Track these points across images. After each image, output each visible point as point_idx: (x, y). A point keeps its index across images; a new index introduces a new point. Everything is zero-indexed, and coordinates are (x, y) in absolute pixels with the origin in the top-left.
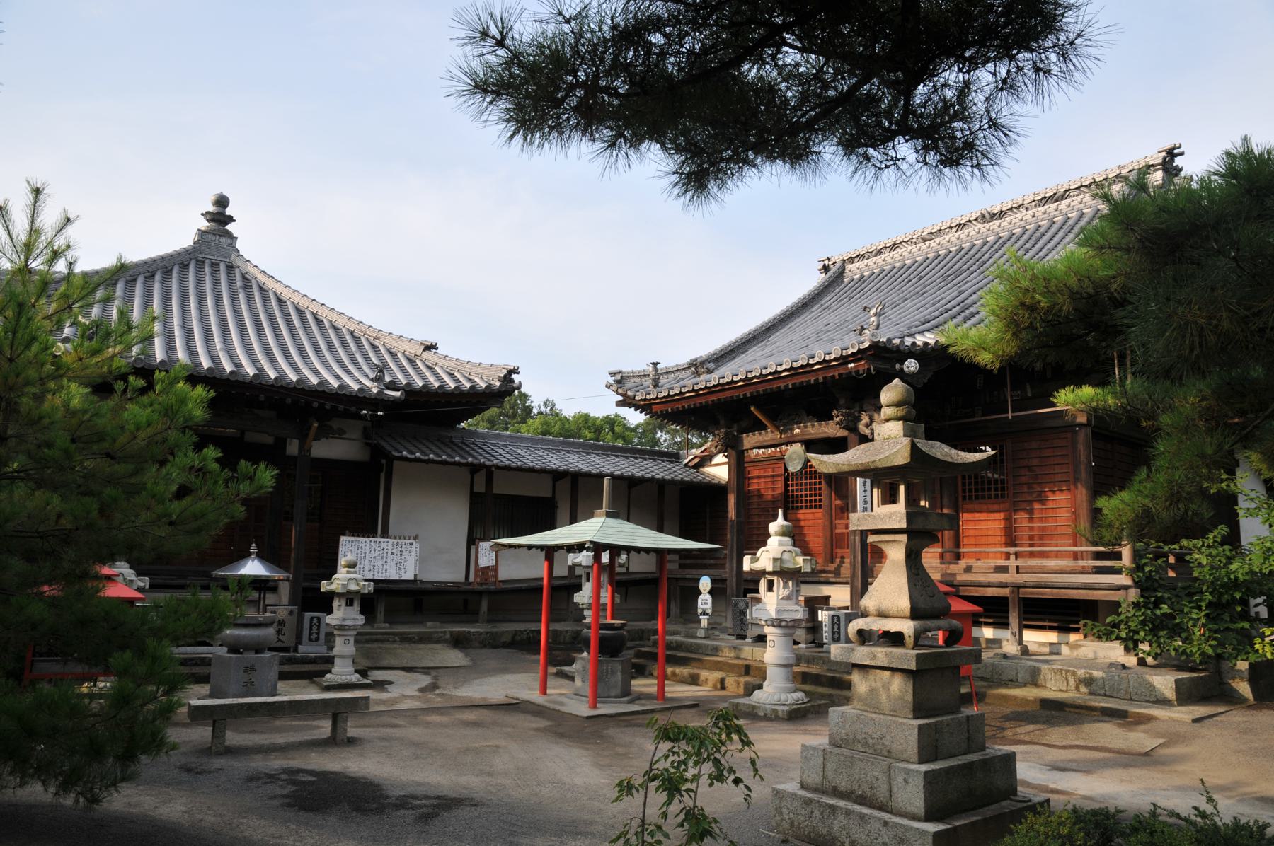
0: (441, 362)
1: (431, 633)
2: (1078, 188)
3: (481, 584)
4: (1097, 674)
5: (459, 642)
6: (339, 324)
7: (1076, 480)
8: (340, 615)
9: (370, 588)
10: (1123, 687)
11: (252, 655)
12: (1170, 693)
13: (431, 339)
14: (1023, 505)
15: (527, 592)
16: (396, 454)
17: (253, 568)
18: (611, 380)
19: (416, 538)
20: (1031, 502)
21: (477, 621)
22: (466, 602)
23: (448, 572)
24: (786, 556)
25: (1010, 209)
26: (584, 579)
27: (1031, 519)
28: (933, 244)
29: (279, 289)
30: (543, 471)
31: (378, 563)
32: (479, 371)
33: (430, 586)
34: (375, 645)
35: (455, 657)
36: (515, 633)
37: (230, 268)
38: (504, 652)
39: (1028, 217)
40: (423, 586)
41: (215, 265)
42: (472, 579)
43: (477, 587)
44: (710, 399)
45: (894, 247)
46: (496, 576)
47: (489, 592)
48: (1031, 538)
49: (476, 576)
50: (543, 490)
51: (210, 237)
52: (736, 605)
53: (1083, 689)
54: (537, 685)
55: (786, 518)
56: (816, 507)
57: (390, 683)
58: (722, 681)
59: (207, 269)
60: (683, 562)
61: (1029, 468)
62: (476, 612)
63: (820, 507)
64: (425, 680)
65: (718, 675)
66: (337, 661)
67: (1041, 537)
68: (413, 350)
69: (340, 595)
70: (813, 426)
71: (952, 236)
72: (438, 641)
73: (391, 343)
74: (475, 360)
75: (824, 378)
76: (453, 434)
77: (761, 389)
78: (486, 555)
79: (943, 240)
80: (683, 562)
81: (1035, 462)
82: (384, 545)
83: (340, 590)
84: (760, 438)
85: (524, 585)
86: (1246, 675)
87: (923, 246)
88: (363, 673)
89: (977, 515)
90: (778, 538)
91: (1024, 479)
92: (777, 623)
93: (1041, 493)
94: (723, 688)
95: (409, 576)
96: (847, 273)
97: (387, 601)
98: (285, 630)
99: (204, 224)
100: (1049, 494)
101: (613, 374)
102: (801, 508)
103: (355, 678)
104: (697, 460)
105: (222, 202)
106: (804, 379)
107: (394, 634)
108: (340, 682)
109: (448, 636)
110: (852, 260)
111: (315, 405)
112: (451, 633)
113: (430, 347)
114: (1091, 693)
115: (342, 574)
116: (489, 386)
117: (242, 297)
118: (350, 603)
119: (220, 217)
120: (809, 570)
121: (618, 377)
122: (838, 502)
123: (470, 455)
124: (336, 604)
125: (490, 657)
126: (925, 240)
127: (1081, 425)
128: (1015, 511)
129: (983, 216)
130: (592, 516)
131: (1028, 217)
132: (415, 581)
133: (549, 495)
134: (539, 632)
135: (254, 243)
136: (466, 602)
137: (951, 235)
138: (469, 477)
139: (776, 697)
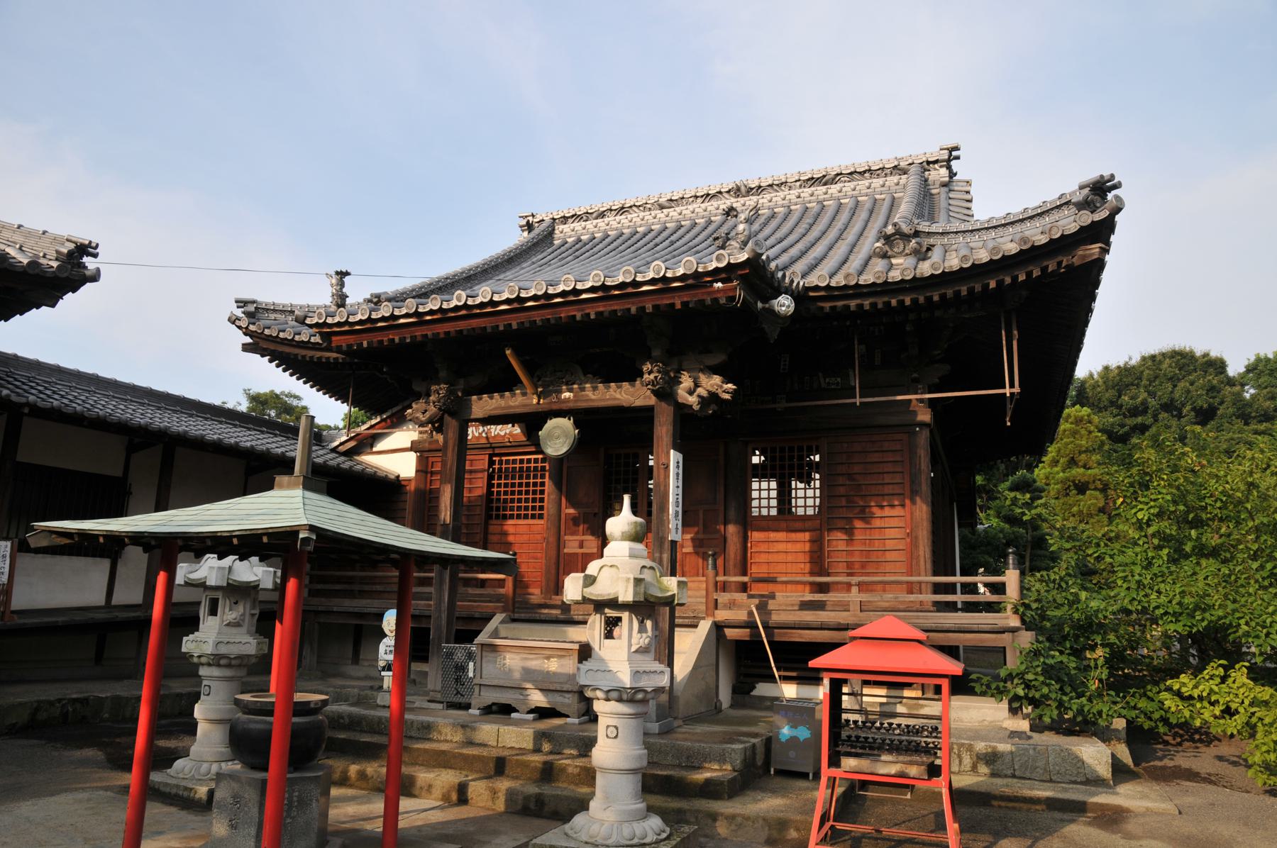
2: (851, 173)
4: (1004, 747)
7: (914, 493)
10: (1040, 764)
12: (1105, 771)
14: (840, 524)
18: (239, 313)
20: (850, 520)
24: (647, 576)
25: (770, 186)
26: (203, 611)
27: (850, 541)
28: (674, 213)
32: (19, 238)
36: (38, 707)
39: (794, 199)
44: (442, 329)
45: (622, 210)
48: (850, 565)
50: (104, 460)
52: (450, 655)
53: (983, 769)
55: (635, 513)
56: (533, 517)
58: (462, 789)
61: (850, 476)
63: (541, 517)
65: (446, 779)
67: (864, 565)
70: (595, 389)
71: (698, 207)
75: (655, 307)
77: (538, 317)
79: (687, 210)
81: (857, 469)
84: (503, 403)
85: (60, 619)
86: (1123, 735)
87: (661, 215)
89: (773, 535)
90: (626, 545)
91: (842, 490)
92: (217, 660)
93: (863, 509)
94: (463, 799)
96: (557, 233)
100: (875, 510)
101: (242, 303)
102: (512, 517)
104: (352, 444)
106: (617, 306)
110: (565, 219)
114: (994, 775)
121: (251, 308)
122: (571, 511)
126: (662, 207)
127: (923, 425)
128: (830, 530)
129: (738, 189)
130: (269, 486)
131: (794, 199)
133: (118, 472)
137: (695, 205)
139: (626, 831)
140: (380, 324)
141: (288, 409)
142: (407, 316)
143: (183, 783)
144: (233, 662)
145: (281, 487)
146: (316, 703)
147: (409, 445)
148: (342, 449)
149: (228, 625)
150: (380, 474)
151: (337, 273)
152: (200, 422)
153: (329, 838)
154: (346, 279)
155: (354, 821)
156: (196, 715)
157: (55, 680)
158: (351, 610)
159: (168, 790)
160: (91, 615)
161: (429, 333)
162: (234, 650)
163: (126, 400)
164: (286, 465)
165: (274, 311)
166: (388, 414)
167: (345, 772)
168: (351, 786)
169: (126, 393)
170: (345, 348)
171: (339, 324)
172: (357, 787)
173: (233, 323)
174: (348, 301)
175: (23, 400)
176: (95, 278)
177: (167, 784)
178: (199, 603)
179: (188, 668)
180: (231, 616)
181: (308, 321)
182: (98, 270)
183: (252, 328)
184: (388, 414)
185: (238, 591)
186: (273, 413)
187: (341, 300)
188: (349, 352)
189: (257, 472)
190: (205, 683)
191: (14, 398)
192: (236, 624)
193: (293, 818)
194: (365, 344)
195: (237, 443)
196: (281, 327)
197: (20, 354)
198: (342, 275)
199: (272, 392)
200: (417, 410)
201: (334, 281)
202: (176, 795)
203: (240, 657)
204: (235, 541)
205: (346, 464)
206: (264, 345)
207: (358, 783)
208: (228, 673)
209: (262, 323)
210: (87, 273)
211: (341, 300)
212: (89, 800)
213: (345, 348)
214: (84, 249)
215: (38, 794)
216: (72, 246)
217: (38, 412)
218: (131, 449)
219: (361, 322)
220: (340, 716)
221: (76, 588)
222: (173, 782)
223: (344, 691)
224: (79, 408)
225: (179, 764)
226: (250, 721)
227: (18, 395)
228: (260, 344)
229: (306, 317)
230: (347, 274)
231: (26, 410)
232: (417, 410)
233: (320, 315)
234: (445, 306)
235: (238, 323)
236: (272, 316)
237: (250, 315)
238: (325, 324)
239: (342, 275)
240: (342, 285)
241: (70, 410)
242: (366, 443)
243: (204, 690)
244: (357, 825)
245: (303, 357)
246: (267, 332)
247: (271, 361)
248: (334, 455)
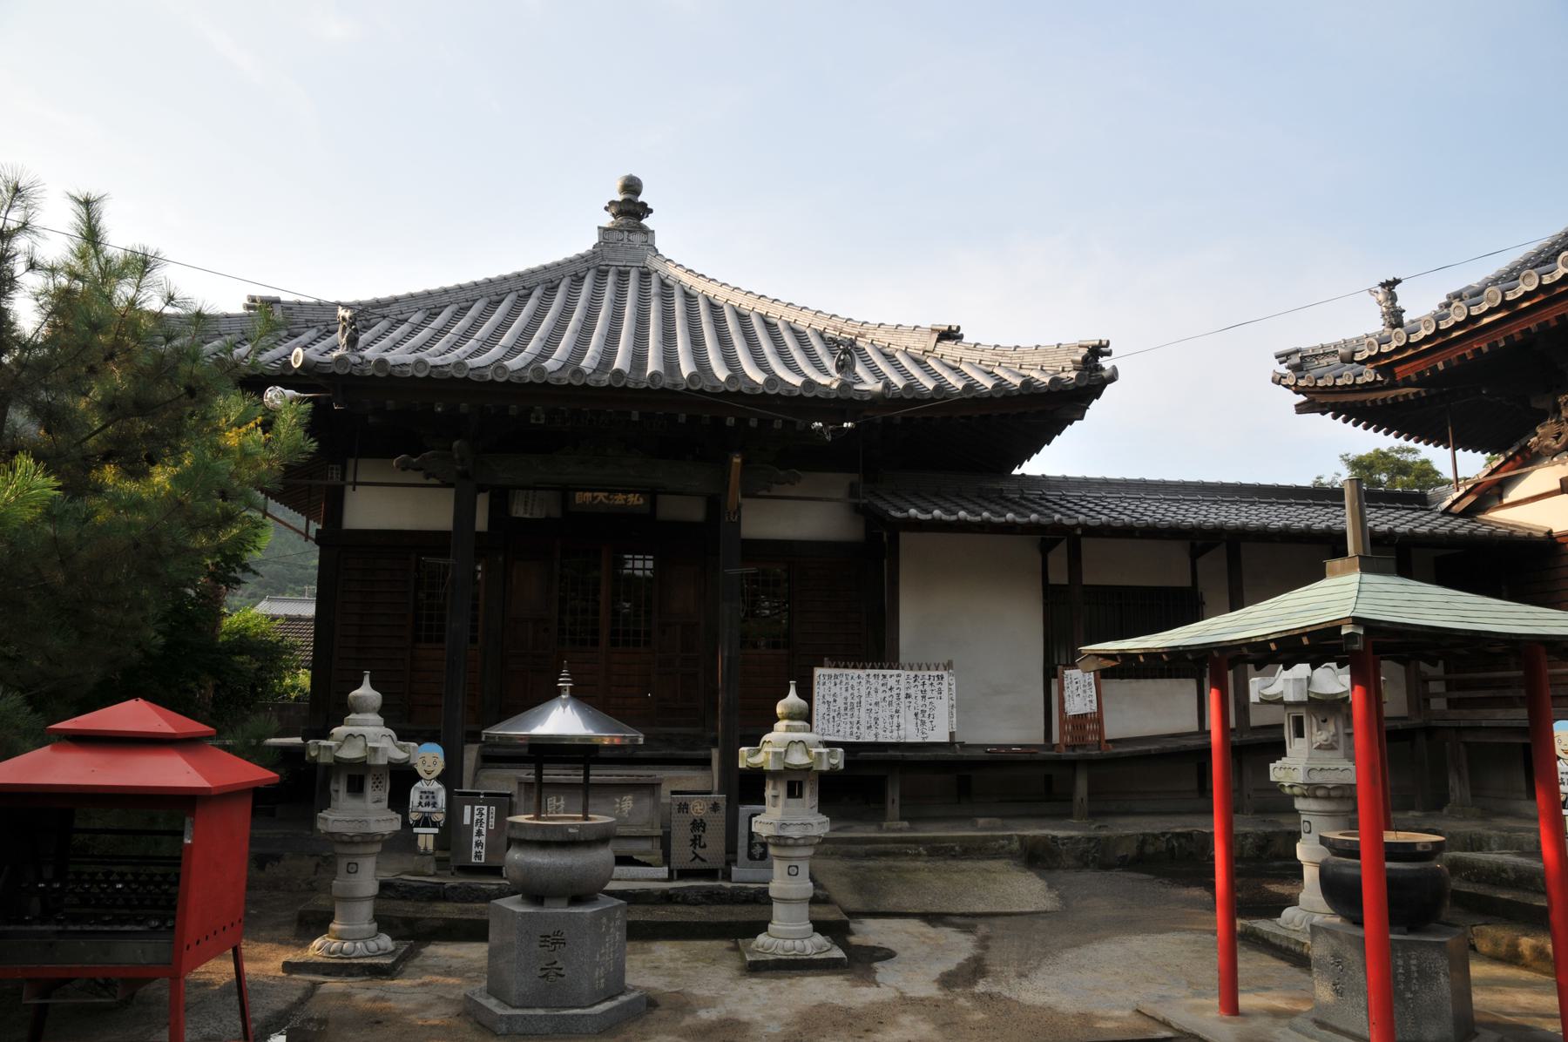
0: (968, 356)
1: (985, 839)
3: (1073, 748)
5: (1036, 857)
6: (802, 324)
8: (773, 816)
9: (838, 759)
11: (561, 909)
13: (944, 323)
15: (1178, 762)
16: (898, 514)
17: (561, 720)
18: (1283, 369)
19: (948, 666)
21: (1070, 815)
22: (1048, 779)
23: (1012, 725)
26: (1288, 733)
29: (712, 290)
31: (884, 713)
32: (1038, 359)
33: (981, 753)
34: (882, 863)
35: (1026, 891)
36: (1144, 840)
37: (645, 275)
38: (1125, 878)
40: (966, 754)
41: (623, 275)
42: (1056, 739)
43: (1066, 753)
46: (1100, 732)
47: (1090, 763)
49: (1062, 733)
50: (1170, 571)
51: (617, 235)
54: (1209, 972)
57: (888, 955)
59: (611, 279)
60: (1456, 695)
62: (1068, 798)
64: (958, 947)
66: (778, 909)
68: (916, 344)
69: (775, 775)
72: (996, 855)
73: (883, 339)
74: (1027, 342)
76: (1004, 485)
78: (1079, 692)
80: (1456, 695)
82: (891, 682)
83: (770, 766)
85: (1153, 747)
88: (833, 930)
92: (1312, 790)
95: (940, 735)
97: (863, 781)
98: (706, 838)
99: (607, 220)
101: (1283, 357)
103: (815, 945)
105: (632, 186)
107: (916, 841)
108: (781, 954)
109: (1016, 846)
112: (1022, 839)
113: (950, 335)
115: (779, 734)
116: (1055, 381)
118: (794, 791)
119: (631, 208)
121: (1296, 360)
123: (1034, 511)
124: (769, 792)
125: (1100, 893)
130: (1319, 575)
132: (951, 744)
133: (1187, 583)
134: (1207, 839)
135: (681, 242)
136: (1048, 779)
138: (1039, 558)
140: (1455, 334)
141: (1403, 469)
142: (1491, 311)
143: (1294, 936)
144: (1333, 793)
145: (1335, 574)
146: (1425, 845)
147: (1558, 486)
148: (1456, 508)
149: (1319, 748)
150: (1520, 533)
151: (1383, 285)
152: (1263, 508)
153: (1479, 1030)
154: (1397, 289)
155: (1527, 1015)
156: (1299, 856)
157: (1180, 813)
158: (1508, 724)
159: (1277, 942)
160: (1184, 742)
161: (1533, 326)
162: (1332, 779)
163: (1178, 501)
164: (1333, 544)
165: (1325, 354)
166: (1515, 448)
167: (1514, 946)
168: (1526, 966)
169: (1177, 493)
170: (1413, 377)
171: (1398, 350)
172: (1535, 970)
173: (1279, 383)
174: (1406, 318)
175: (1074, 522)
176: (1113, 378)
177: (1276, 935)
178: (1281, 726)
179: (1279, 802)
180: (1321, 737)
181: (1358, 357)
182: (1114, 368)
183: (1302, 383)
184: (1515, 448)
185: (1326, 707)
186: (1384, 478)
187: (1395, 318)
188: (1421, 381)
189: (1305, 556)
190: (1304, 818)
191: (1066, 521)
192: (1329, 747)
193: (1414, 993)
194: (1441, 366)
195: (1308, 527)
196: (1337, 372)
197: (1069, 475)
198: (1389, 285)
199: (1377, 450)
200: (1546, 436)
201: (1381, 297)
202: (1287, 949)
203: (1338, 787)
204: (1273, 646)
205: (1463, 527)
206: (1322, 399)
207: (1536, 964)
208: (1329, 806)
209: (1312, 374)
210: (1105, 374)
211: (1395, 318)
212: (1196, 942)
213: (1413, 377)
214: (1097, 351)
215: (1147, 930)
216: (1085, 351)
217: (1089, 531)
218: (1046, 549)
219: (1427, 339)
220: (1501, 869)
221: (1159, 713)
222: (1283, 933)
223: (1514, 836)
224: (1127, 519)
225: (1288, 912)
226: (1341, 865)
227: (1070, 517)
228: (1319, 400)
229: (1353, 353)
230: (1397, 282)
231: (1079, 532)
232: (1546, 436)
233: (1370, 345)
234: (1547, 280)
235: (1284, 381)
236: (1324, 362)
237: (1296, 368)
238: (1380, 355)
239: (1389, 285)
240: (1393, 298)
241: (1118, 523)
242: (1490, 493)
243: (1304, 827)
244: (1529, 1022)
245: (1374, 402)
246: (1320, 383)
247: (1335, 417)
248: (1447, 518)
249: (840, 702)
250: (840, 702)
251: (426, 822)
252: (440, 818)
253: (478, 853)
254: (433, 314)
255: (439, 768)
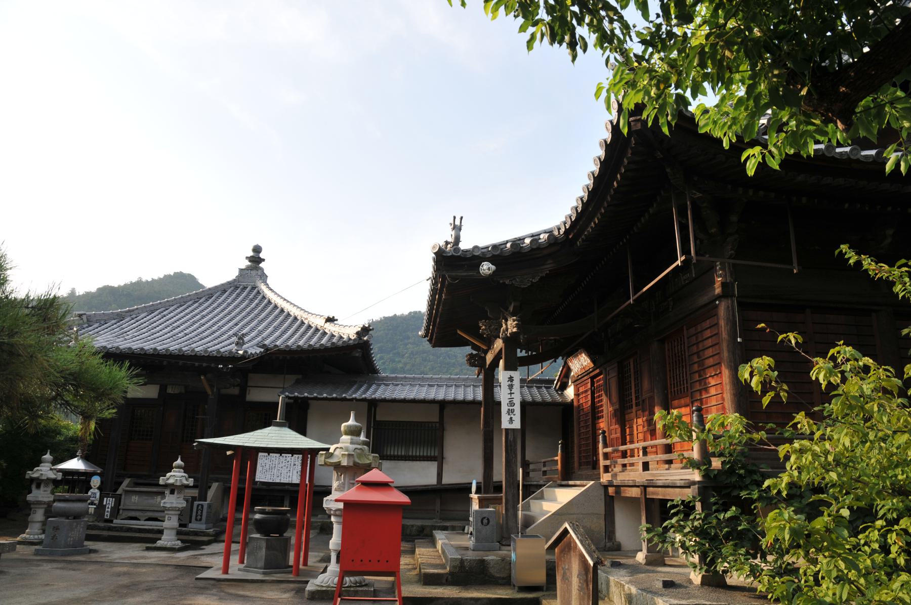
30: (433, 402)
31: (284, 471)
66: (165, 532)
90: (349, 437)
105: (257, 250)
111: (165, 363)
113: (330, 320)
117: (247, 302)
119: (256, 259)
120: (345, 464)
249: (267, 466)
250: (267, 466)
251: (92, 503)
252: (97, 502)
253: (107, 515)
254: (225, 291)
255: (98, 485)
